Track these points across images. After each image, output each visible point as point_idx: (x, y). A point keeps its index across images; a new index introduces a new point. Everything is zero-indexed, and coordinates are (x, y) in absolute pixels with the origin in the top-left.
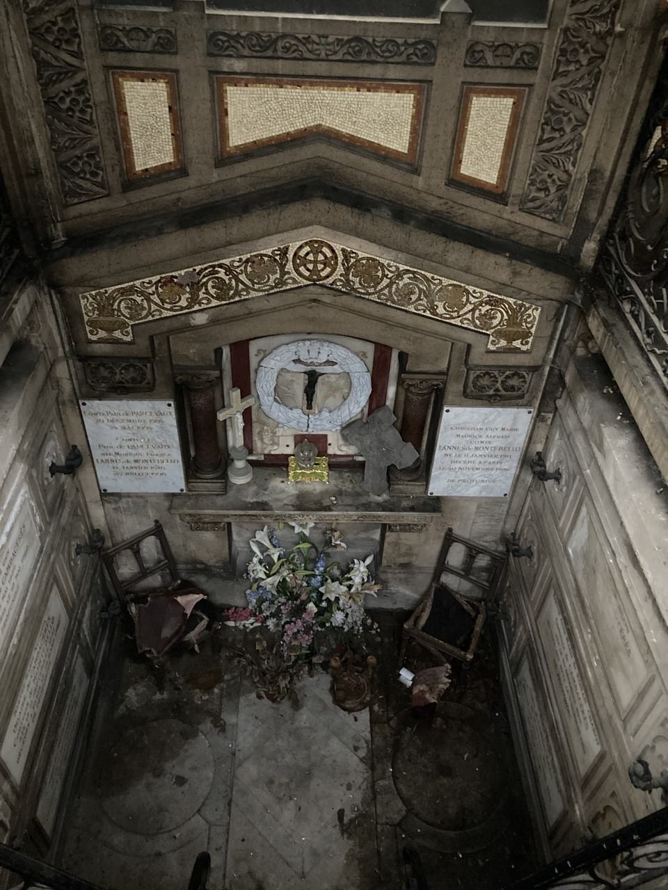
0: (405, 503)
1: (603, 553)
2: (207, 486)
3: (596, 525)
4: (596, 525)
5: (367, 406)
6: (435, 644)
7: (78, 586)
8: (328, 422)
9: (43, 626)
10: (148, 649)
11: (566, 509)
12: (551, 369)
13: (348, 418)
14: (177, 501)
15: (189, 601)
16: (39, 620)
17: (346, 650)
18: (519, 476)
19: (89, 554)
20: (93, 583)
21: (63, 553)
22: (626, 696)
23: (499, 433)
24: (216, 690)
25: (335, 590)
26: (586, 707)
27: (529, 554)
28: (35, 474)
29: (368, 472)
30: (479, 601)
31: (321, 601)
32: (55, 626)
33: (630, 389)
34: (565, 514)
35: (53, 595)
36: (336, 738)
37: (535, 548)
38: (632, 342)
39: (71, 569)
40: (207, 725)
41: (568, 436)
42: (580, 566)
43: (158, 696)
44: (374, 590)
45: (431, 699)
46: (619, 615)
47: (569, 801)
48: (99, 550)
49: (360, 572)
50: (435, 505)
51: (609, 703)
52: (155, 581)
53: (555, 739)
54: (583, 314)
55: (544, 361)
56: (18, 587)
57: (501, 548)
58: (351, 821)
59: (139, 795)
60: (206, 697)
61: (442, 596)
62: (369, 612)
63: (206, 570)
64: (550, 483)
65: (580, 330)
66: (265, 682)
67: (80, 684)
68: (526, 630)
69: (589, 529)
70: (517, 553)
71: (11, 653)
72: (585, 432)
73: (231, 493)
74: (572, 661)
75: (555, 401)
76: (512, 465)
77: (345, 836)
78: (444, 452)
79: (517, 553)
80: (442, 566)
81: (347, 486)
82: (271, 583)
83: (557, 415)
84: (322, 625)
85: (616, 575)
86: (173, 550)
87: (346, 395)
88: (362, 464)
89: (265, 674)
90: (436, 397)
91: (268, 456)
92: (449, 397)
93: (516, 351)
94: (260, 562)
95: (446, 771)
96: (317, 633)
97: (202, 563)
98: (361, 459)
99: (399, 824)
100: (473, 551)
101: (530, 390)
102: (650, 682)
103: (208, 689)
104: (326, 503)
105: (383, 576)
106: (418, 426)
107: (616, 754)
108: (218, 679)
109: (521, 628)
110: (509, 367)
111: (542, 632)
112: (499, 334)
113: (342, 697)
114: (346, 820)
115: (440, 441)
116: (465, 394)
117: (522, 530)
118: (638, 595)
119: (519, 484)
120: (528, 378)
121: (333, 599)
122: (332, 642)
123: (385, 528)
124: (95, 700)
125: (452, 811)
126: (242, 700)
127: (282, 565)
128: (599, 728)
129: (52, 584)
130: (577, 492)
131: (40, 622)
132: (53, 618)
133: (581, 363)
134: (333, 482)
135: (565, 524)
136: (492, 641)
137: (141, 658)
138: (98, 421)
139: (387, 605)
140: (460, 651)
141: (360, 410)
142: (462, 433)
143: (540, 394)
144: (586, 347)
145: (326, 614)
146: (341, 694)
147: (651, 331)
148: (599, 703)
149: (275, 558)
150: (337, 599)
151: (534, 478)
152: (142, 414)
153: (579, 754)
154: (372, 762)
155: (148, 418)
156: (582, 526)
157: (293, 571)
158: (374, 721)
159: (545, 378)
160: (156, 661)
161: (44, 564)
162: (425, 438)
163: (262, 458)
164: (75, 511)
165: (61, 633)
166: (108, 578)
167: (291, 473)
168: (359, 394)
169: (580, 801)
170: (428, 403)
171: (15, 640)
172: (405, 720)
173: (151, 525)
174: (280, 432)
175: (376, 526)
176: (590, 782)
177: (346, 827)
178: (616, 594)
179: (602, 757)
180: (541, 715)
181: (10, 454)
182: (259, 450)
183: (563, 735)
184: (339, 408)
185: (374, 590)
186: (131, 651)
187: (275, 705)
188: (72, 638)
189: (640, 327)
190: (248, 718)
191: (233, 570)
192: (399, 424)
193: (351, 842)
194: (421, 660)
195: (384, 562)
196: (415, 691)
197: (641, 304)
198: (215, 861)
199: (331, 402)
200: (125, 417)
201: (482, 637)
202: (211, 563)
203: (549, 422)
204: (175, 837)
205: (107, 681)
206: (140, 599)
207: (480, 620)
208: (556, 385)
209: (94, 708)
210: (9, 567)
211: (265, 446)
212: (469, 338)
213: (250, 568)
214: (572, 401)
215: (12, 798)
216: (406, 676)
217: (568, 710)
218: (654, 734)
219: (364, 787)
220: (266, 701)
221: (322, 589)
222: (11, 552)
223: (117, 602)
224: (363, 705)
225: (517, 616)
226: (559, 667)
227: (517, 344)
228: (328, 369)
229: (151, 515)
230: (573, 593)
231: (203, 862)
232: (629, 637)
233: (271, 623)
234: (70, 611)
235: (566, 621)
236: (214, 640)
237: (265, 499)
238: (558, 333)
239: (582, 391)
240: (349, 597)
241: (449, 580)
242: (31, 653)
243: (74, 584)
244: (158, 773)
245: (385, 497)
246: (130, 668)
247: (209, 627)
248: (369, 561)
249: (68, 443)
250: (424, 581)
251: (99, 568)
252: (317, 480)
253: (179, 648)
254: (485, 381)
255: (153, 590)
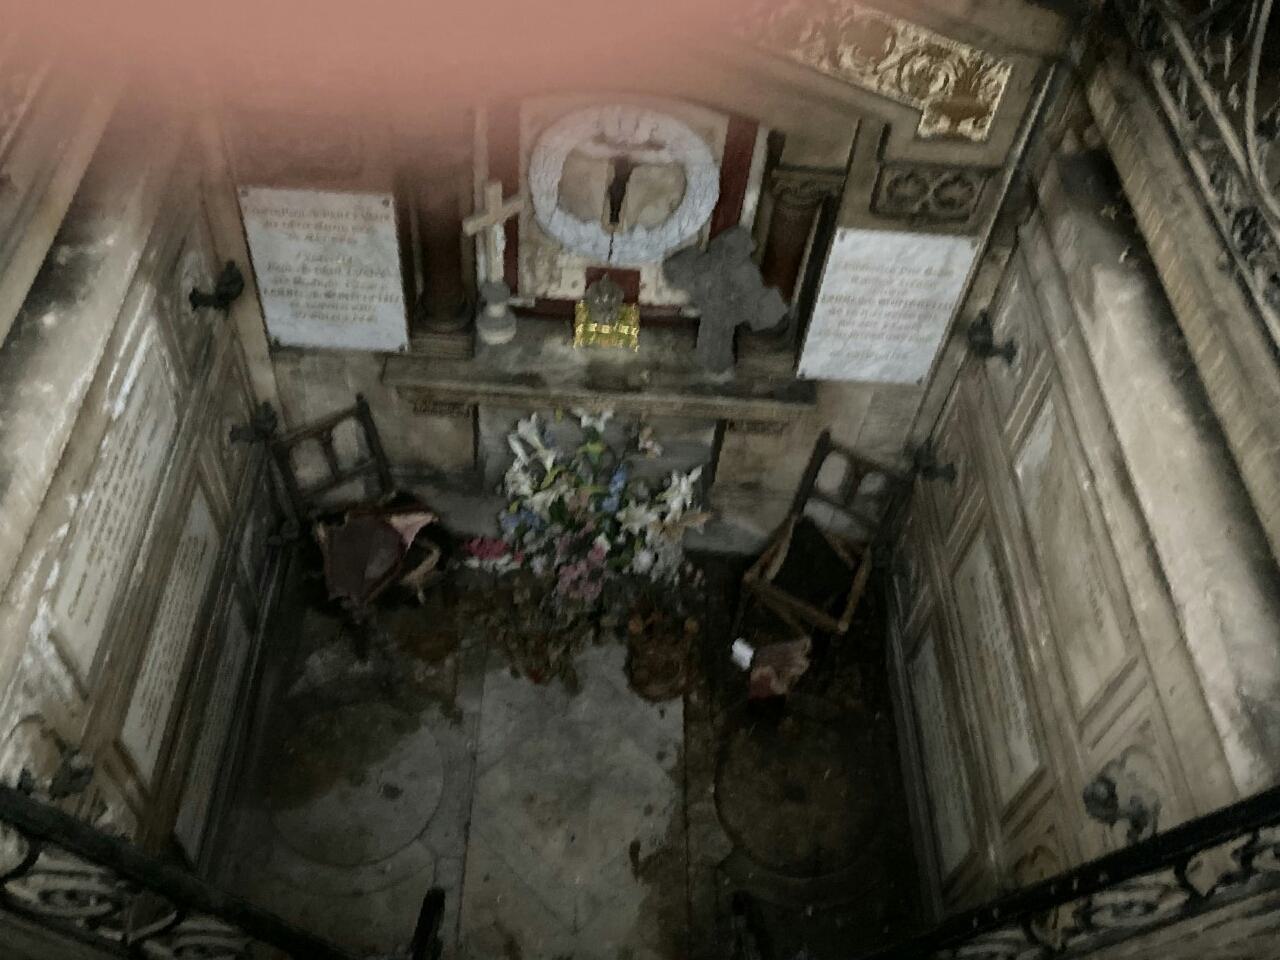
0: (759, 387)
1: (1073, 472)
2: (443, 342)
3: (1067, 429)
4: (1067, 429)
5: (709, 226)
6: (787, 606)
7: (234, 492)
8: (642, 250)
9: (181, 551)
10: (345, 594)
11: (1019, 404)
12: (1017, 174)
13: (678, 241)
14: (392, 365)
15: (410, 524)
16: (174, 541)
17: (652, 610)
18: (945, 350)
19: (252, 442)
20: (255, 490)
21: (211, 437)
22: (1088, 687)
23: (921, 277)
24: (449, 662)
25: (640, 517)
26: (1022, 705)
27: (950, 474)
28: (167, 303)
29: (705, 334)
30: (864, 545)
31: (618, 533)
32: (199, 549)
33: (1150, 208)
34: (1015, 412)
35: (195, 502)
36: (636, 739)
37: (960, 467)
38: (1159, 130)
39: (222, 461)
40: (434, 713)
41: (1033, 287)
42: (1032, 494)
43: (357, 668)
44: (700, 520)
45: (779, 688)
46: (1089, 568)
47: (980, 840)
48: (267, 435)
49: (680, 492)
50: (807, 391)
51: (1059, 699)
52: (355, 491)
53: (967, 753)
54: (1080, 81)
55: (1008, 156)
56: (143, 484)
57: (904, 465)
58: (650, 858)
59: (329, 809)
60: (432, 672)
61: (805, 533)
62: (689, 554)
63: (437, 478)
64: (995, 363)
65: (1073, 106)
66: (526, 652)
67: (236, 650)
68: (933, 590)
69: (1054, 438)
70: (930, 472)
71: (134, 588)
72: (1064, 280)
73: (482, 356)
74: (1004, 637)
75: (1017, 229)
76: (936, 332)
77: (640, 880)
78: (828, 306)
79: (930, 472)
80: (808, 488)
81: (668, 356)
82: (540, 501)
83: (1018, 252)
84: (618, 569)
85: (1092, 507)
86: (384, 440)
87: (675, 203)
88: (695, 323)
89: (525, 640)
90: (824, 217)
91: (543, 301)
92: (846, 213)
93: (964, 140)
94: (525, 469)
95: (795, 794)
96: (608, 583)
97: (431, 467)
98: (692, 313)
99: (722, 865)
100: (859, 467)
101: (978, 209)
102: (1128, 669)
103: (435, 659)
104: (633, 380)
105: (714, 502)
106: (792, 260)
107: (1061, 773)
108: (452, 646)
109: (926, 588)
110: (944, 167)
111: (961, 593)
112: (939, 109)
113: (642, 679)
114: (642, 856)
115: (825, 288)
116: (873, 208)
117: (942, 436)
118: (1125, 538)
119: (943, 365)
120: (978, 188)
121: (636, 530)
122: (631, 596)
123: (723, 426)
124: (260, 670)
125: (802, 849)
126: (489, 678)
127: (559, 475)
128: (1040, 735)
129: (194, 488)
130: (1040, 378)
131: (177, 543)
132: (196, 539)
133: (1067, 165)
134: (646, 349)
135: (1013, 431)
136: (877, 609)
137: (333, 609)
138: (267, 224)
139: (717, 545)
140: (832, 620)
141: (698, 228)
142: (863, 274)
143: (993, 217)
144: (1080, 137)
145: (624, 555)
146: (643, 674)
147: (1196, 110)
148: (1043, 699)
149: (549, 464)
150: (643, 533)
151: (969, 354)
152: (340, 215)
153: (1002, 771)
154: (684, 776)
155: (350, 223)
156: (1042, 431)
157: (577, 485)
158: (689, 717)
159: (1005, 191)
160: (356, 613)
161: (182, 453)
162: (800, 281)
163: (532, 303)
164: (230, 371)
165: (210, 559)
166: (281, 485)
167: (579, 329)
168: (698, 202)
169: (998, 837)
170: (810, 224)
171: (140, 566)
172: (739, 717)
173: (350, 402)
174: (562, 261)
175: (706, 423)
176: (1019, 812)
177: (643, 866)
178: (1089, 533)
179: (1039, 777)
180: (948, 719)
181: (129, 267)
182: (528, 290)
183: (980, 746)
184: (664, 222)
185: (700, 520)
186: (317, 596)
187: (540, 687)
188: (223, 574)
189: (1177, 100)
190: (498, 704)
191: (480, 480)
192: (759, 257)
193: (648, 887)
194: (766, 630)
195: (718, 478)
196: (756, 675)
197: (1183, 64)
198: (450, 904)
199: (651, 213)
200: (312, 221)
201: (862, 601)
202: (446, 467)
203: (1003, 263)
204: (383, 872)
205: (277, 645)
206: (332, 517)
207: (863, 574)
208: (1024, 201)
209: (258, 681)
210: (129, 450)
211: (536, 284)
212: (890, 112)
213: (509, 477)
214: (1047, 228)
215: (136, 797)
216: (742, 652)
217: (993, 713)
218: (1125, 744)
219: (671, 811)
220: (525, 681)
221: (621, 516)
222: (132, 427)
223: (295, 522)
224: (673, 693)
225: (922, 569)
226: (983, 648)
227: (966, 127)
228: (650, 156)
229: (350, 386)
230: (1017, 534)
231: (434, 902)
232: (1103, 601)
233: (538, 564)
234: (223, 528)
235: (1003, 578)
236: (448, 587)
237: (535, 368)
238: (1035, 112)
239: (1065, 210)
240: (663, 525)
241: (818, 511)
242: (164, 592)
243: (227, 487)
244: (358, 779)
245: (726, 377)
246: (313, 621)
247: (440, 565)
248: (695, 475)
249: (217, 257)
250: (777, 510)
251: (265, 467)
252: (617, 340)
253: (394, 596)
254: (908, 189)
255: (353, 506)
